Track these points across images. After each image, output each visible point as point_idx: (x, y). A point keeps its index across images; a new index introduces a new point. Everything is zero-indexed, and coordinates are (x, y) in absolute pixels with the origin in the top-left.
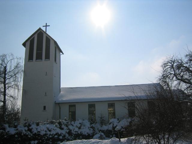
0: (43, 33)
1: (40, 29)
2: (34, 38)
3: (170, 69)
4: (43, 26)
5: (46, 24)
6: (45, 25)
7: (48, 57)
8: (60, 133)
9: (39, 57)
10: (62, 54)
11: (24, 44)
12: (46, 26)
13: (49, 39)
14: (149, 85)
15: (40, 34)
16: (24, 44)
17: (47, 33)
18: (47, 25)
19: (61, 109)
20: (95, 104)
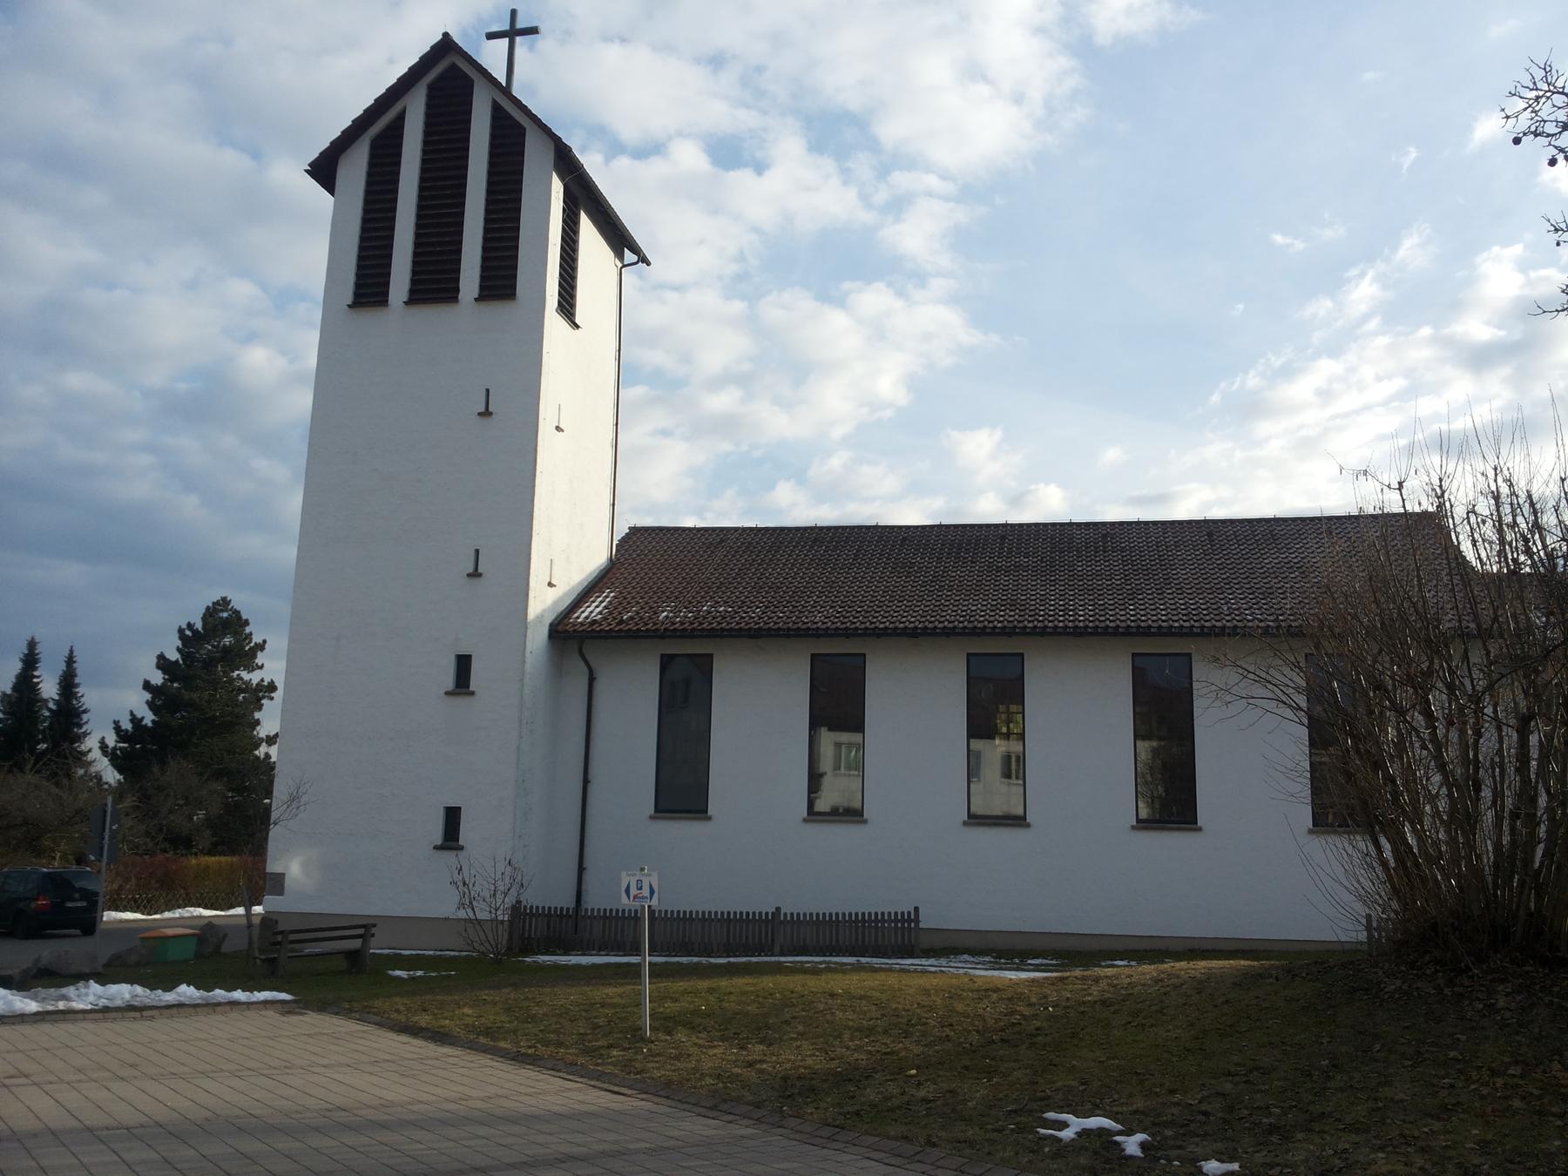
0: (521, 132)
1: (446, 46)
2: (401, 118)
3: (1494, 488)
4: (491, 36)
5: (514, 13)
6: (507, 27)
7: (501, 280)
8: (1444, 410)
9: (435, 284)
10: (635, 258)
11: (324, 170)
12: (513, 33)
13: (515, 128)
14: (347, 1013)
15: (445, 76)
16: (324, 170)
17: (516, 91)
18: (520, 25)
19: (592, 788)
20: (711, 656)
